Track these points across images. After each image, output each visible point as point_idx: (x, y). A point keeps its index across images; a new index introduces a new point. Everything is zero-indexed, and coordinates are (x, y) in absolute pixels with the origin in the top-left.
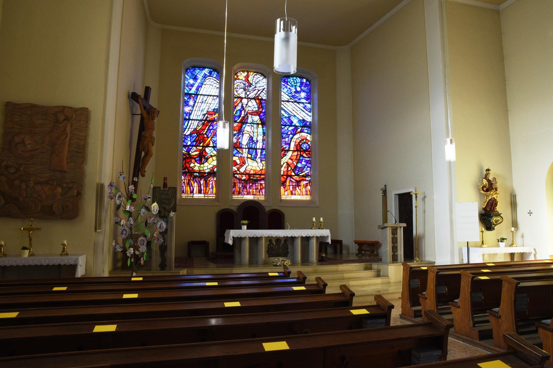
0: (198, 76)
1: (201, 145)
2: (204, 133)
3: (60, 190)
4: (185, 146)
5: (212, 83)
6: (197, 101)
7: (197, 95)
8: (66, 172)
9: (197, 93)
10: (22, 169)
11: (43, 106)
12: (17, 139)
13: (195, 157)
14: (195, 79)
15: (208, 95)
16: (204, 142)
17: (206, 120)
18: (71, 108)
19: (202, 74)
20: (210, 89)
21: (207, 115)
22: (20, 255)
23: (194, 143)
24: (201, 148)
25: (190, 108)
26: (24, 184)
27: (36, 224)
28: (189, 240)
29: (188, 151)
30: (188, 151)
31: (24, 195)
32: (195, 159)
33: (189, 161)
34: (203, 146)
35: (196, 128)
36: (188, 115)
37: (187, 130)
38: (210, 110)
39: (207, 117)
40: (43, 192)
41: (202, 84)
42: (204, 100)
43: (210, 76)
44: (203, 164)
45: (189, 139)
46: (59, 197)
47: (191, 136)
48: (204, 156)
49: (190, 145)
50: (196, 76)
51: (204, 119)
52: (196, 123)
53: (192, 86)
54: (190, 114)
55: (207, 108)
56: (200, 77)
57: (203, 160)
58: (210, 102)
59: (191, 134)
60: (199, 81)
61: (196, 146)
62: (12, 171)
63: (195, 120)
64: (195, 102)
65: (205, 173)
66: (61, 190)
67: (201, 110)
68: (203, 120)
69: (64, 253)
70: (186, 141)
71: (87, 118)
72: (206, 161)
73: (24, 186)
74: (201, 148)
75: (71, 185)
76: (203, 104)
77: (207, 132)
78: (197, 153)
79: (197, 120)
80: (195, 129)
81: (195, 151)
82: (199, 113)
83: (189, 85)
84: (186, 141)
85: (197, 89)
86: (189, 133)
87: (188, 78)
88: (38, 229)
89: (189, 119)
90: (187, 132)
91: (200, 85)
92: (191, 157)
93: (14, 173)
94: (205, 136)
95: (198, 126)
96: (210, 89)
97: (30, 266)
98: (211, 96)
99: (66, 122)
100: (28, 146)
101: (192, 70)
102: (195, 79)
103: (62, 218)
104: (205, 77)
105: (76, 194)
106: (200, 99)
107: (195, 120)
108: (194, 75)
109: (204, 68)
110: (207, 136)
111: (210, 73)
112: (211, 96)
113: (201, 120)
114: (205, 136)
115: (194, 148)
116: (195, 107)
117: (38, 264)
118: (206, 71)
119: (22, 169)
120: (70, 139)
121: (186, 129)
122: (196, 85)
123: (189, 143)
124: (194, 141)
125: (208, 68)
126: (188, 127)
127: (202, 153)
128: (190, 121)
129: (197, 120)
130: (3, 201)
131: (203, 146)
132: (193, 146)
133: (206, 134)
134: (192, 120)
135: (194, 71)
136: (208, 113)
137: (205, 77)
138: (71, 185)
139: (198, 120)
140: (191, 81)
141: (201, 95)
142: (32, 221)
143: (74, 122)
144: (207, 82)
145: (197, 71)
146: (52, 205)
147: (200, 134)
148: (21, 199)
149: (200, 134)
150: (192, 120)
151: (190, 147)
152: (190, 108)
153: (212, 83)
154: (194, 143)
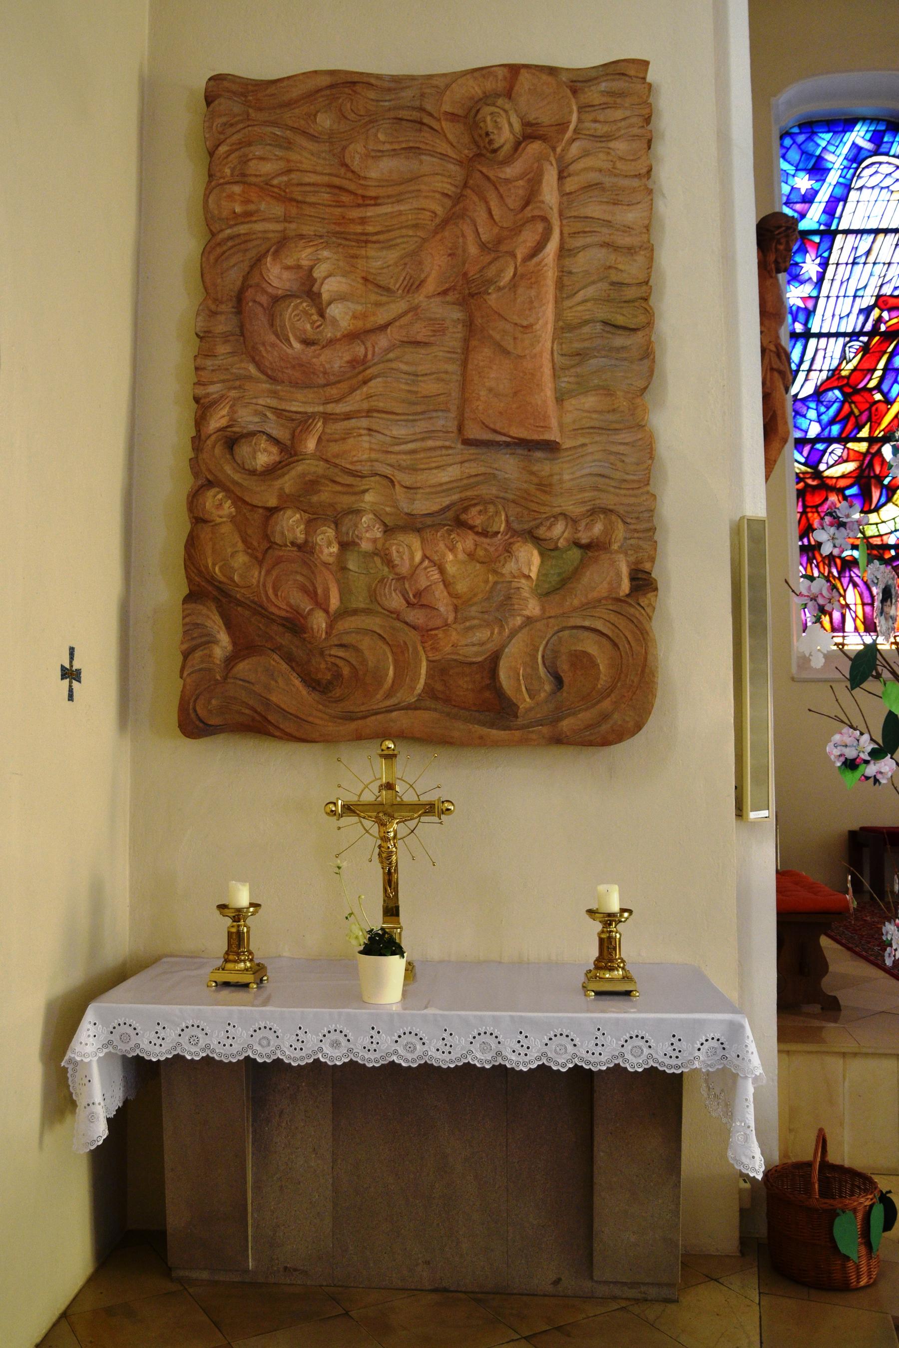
0: (829, 157)
1: (864, 433)
2: (872, 384)
3: (529, 560)
4: (800, 443)
5: (888, 181)
6: (833, 260)
7: (829, 234)
8: (551, 447)
9: (829, 225)
10: (311, 445)
11: (396, 79)
12: (277, 276)
13: (842, 483)
14: (818, 170)
15: (876, 232)
16: (875, 422)
17: (871, 334)
18: (552, 71)
19: (845, 150)
20: (881, 205)
21: (876, 313)
22: (353, 995)
23: (835, 429)
24: (863, 447)
25: (807, 290)
26: (330, 533)
27: (420, 775)
28: (855, 826)
29: (813, 461)
30: (813, 461)
31: (334, 602)
32: (841, 491)
33: (818, 500)
34: (871, 440)
35: (838, 369)
36: (801, 317)
37: (801, 376)
38: (887, 290)
39: (880, 320)
40: (435, 576)
41: (848, 188)
42: (862, 250)
43: (876, 153)
44: (877, 510)
45: (812, 414)
46: (533, 608)
47: (819, 402)
48: (880, 479)
49: (818, 439)
50: (820, 158)
51: (868, 327)
52: (835, 346)
53: (809, 198)
54: (809, 313)
55: (875, 282)
56: (836, 160)
57: (876, 494)
58: (884, 257)
59: (818, 395)
60: (833, 177)
61: (842, 439)
62: (264, 457)
63: (829, 335)
64: (825, 264)
65: (888, 547)
66: (536, 559)
67: (851, 292)
68: (861, 333)
69: (608, 976)
70: (803, 423)
71: (648, 120)
72: (889, 499)
73: (327, 546)
74: (863, 447)
75: (598, 529)
76: (858, 269)
77: (882, 379)
78: (850, 467)
79: (837, 335)
80: (835, 372)
81: (841, 461)
82: (845, 306)
83: (794, 197)
84: (803, 423)
85: (830, 211)
86: (809, 389)
87: (790, 169)
88: (430, 809)
89: (807, 335)
90: (803, 387)
91: (839, 192)
92: (825, 486)
93: (271, 472)
94: (878, 397)
95: (843, 357)
96: (881, 205)
97: (427, 1070)
98: (886, 231)
99: (535, 147)
100: (335, 311)
101: (800, 139)
102: (818, 170)
103: (558, 741)
104: (857, 157)
105: (625, 586)
106: (843, 247)
107: (829, 335)
108: (810, 155)
109: (848, 124)
110: (885, 395)
111: (877, 139)
112: (886, 231)
113: (854, 335)
114: (878, 397)
115: (837, 449)
116: (826, 284)
117: (482, 1058)
118: (859, 135)
119: (311, 445)
120: (564, 252)
121: (797, 371)
122: (823, 196)
123: (814, 430)
124: (832, 422)
125: (864, 119)
126: (805, 366)
127: (871, 465)
128: (813, 342)
129: (837, 335)
130: (224, 638)
131: (871, 440)
132: (830, 441)
133: (878, 388)
134: (819, 335)
135: (810, 139)
136: (881, 301)
137: (857, 157)
138: (598, 529)
139: (844, 335)
140: (803, 183)
141: (847, 232)
142: (390, 757)
143: (575, 149)
144: (867, 177)
145: (824, 138)
146: (495, 659)
147: (857, 392)
148: (319, 621)
149: (857, 392)
150: (819, 335)
151: (820, 446)
152: (807, 290)
153: (888, 181)
154: (835, 429)
